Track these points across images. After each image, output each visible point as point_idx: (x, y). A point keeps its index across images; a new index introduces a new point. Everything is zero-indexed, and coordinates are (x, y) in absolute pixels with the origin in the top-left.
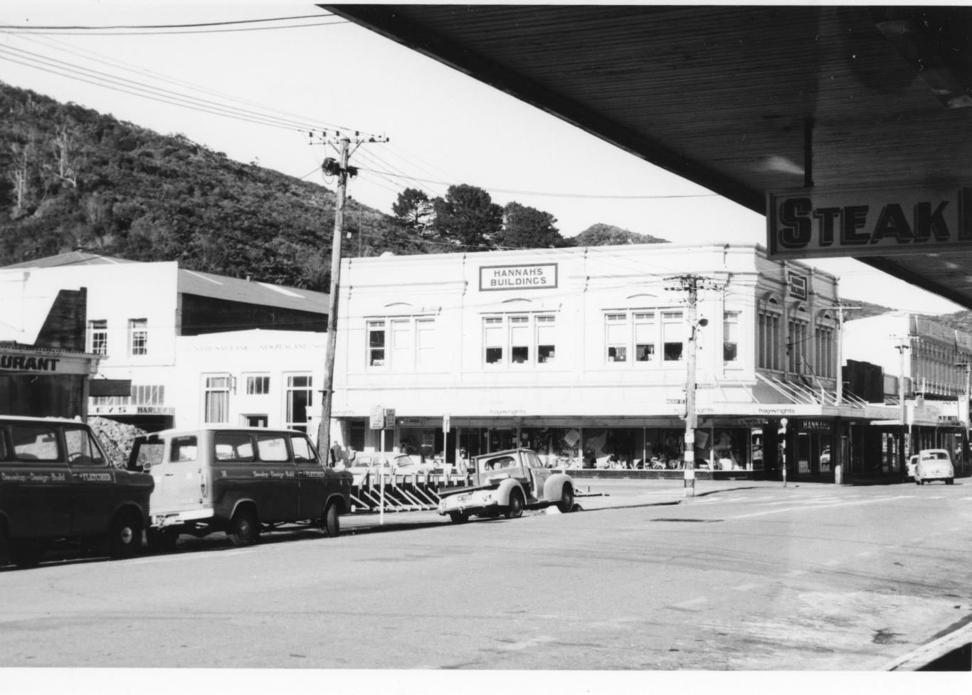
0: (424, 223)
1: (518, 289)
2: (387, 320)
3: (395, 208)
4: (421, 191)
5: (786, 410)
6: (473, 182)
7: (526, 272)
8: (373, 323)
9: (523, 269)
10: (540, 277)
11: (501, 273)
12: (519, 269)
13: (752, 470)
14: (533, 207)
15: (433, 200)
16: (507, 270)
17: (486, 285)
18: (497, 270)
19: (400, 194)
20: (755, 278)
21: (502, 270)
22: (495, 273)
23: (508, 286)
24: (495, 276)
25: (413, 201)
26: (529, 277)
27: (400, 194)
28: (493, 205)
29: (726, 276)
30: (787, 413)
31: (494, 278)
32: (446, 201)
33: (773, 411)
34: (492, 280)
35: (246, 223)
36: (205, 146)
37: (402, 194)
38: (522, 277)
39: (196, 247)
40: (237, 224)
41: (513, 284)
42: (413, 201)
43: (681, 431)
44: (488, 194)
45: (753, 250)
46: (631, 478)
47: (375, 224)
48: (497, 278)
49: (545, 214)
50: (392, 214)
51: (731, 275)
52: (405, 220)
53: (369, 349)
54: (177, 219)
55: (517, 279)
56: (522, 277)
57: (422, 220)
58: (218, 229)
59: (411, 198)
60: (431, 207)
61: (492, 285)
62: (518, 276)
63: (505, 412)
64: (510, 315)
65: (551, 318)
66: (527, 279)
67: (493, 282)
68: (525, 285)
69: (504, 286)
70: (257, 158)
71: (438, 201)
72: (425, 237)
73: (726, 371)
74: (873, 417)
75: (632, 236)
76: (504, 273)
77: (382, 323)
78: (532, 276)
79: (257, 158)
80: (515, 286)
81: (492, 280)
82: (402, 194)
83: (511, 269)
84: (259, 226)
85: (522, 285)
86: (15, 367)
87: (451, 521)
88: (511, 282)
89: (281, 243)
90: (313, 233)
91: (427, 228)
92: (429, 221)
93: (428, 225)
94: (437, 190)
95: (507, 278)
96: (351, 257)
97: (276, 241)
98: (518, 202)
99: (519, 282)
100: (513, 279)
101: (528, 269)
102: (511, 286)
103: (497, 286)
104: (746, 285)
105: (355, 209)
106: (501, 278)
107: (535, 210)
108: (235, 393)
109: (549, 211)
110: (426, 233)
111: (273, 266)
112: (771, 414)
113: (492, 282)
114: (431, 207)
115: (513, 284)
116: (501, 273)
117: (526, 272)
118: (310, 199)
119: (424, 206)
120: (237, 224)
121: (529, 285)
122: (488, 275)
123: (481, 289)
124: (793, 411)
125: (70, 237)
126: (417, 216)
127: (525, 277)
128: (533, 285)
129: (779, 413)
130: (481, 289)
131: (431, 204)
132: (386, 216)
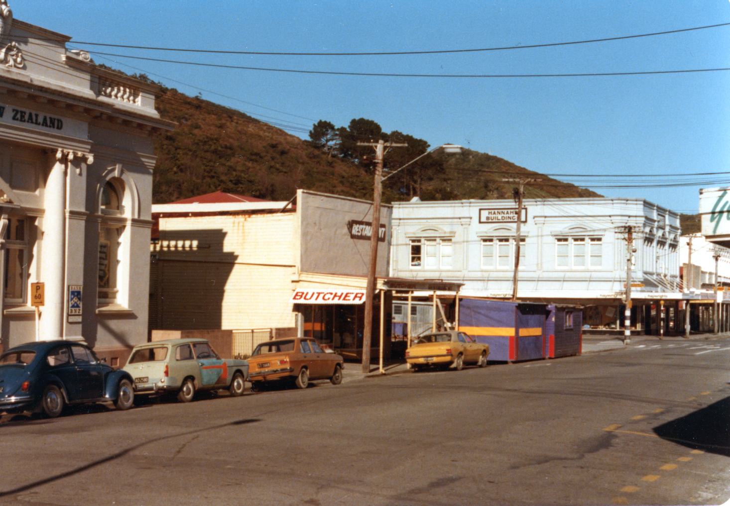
0: (332, 146)
1: (502, 222)
2: (423, 240)
3: (311, 135)
4: (330, 122)
5: (662, 296)
6: (367, 117)
7: (507, 213)
8: (413, 241)
9: (506, 211)
11: (493, 213)
12: (503, 211)
13: (640, 330)
14: (410, 135)
15: (338, 130)
16: (496, 211)
17: (483, 219)
18: (490, 211)
19: (314, 125)
20: (643, 219)
21: (493, 211)
23: (497, 221)
25: (324, 130)
26: (510, 215)
27: (314, 125)
28: (383, 133)
30: (664, 298)
31: (488, 216)
32: (348, 130)
33: (656, 296)
35: (213, 147)
36: (159, 83)
37: (316, 124)
38: (505, 216)
39: (182, 165)
40: (207, 147)
41: (500, 220)
42: (324, 130)
43: (623, 308)
44: (379, 125)
45: (642, 203)
46: (591, 334)
47: (299, 147)
48: (490, 216)
49: (421, 141)
50: (309, 139)
52: (318, 144)
53: (411, 256)
54: (166, 145)
56: (505, 216)
57: (331, 143)
58: (195, 151)
59: (322, 128)
60: (336, 135)
62: (503, 215)
63: (500, 295)
67: (488, 218)
68: (507, 220)
69: (494, 221)
70: (200, 93)
71: (342, 130)
72: (333, 156)
74: (691, 298)
75: (472, 153)
76: (494, 213)
77: (419, 241)
79: (200, 93)
80: (501, 221)
82: (316, 124)
83: (499, 211)
84: (222, 149)
85: (505, 220)
86: (100, 252)
89: (238, 162)
90: (256, 154)
91: (334, 149)
92: (336, 144)
93: (335, 147)
94: (342, 121)
95: (496, 216)
97: (234, 160)
98: (399, 131)
99: (503, 218)
100: (500, 217)
101: (509, 211)
102: (498, 221)
103: (490, 221)
105: (281, 135)
106: (493, 216)
107: (411, 137)
109: (425, 139)
110: (333, 153)
111: (235, 179)
112: (655, 298)
114: (336, 135)
116: (493, 213)
117: (507, 213)
118: (248, 127)
119: (332, 133)
120: (207, 147)
121: (509, 220)
122: (485, 214)
123: (480, 222)
124: (666, 296)
126: (327, 141)
127: (507, 215)
128: (512, 220)
129: (659, 298)
130: (480, 222)
131: (337, 132)
132: (306, 141)
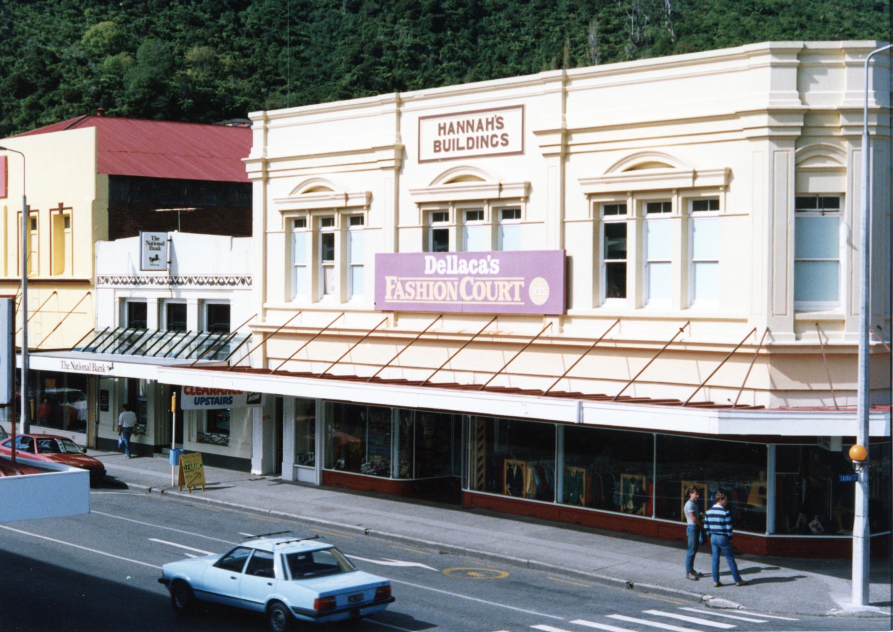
10: (499, 133)
22: (440, 128)
24: (439, 134)
29: (557, 138)
34: (435, 142)
41: (463, 148)
51: (567, 134)
55: (469, 139)
56: (474, 135)
61: (435, 151)
62: (471, 134)
64: (641, 197)
65: (714, 204)
66: (482, 138)
67: (437, 146)
73: (268, 312)
77: (623, 209)
78: (490, 133)
81: (435, 142)
87: (318, 483)
88: (461, 145)
96: (399, 91)
104: (383, 168)
108: (108, 328)
113: (435, 146)
115: (463, 148)
125: (589, 16)
127: (480, 133)
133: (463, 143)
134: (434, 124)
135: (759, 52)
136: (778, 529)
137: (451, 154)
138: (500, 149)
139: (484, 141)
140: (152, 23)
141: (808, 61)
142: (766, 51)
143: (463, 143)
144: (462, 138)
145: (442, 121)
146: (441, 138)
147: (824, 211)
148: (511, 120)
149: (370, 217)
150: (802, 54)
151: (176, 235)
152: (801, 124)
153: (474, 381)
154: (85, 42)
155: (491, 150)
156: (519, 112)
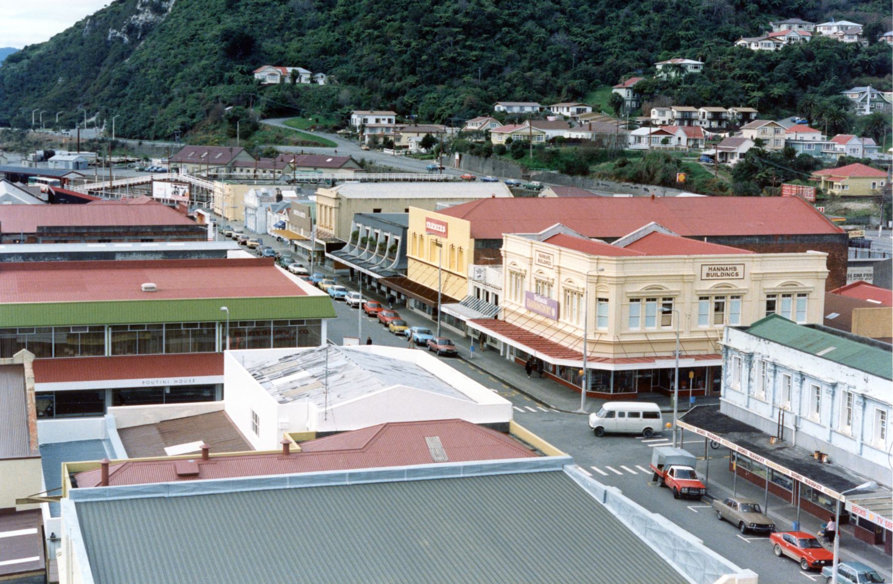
10: (735, 272)
67: (708, 275)
133: (719, 274)
134: (707, 267)
135: (661, 261)
136: (614, 391)
137: (714, 278)
138: (735, 277)
139: (728, 275)
140: (159, 103)
141: (600, 261)
142: (8, 238)
143: (719, 274)
144: (719, 273)
145: (710, 267)
146: (710, 272)
147: (598, 259)
148: (740, 269)
149: (554, 286)
150: (598, 259)
151: (487, 267)
152: (258, 231)
153: (665, 192)
154: (33, 140)
155: (731, 277)
156: (742, 266)
